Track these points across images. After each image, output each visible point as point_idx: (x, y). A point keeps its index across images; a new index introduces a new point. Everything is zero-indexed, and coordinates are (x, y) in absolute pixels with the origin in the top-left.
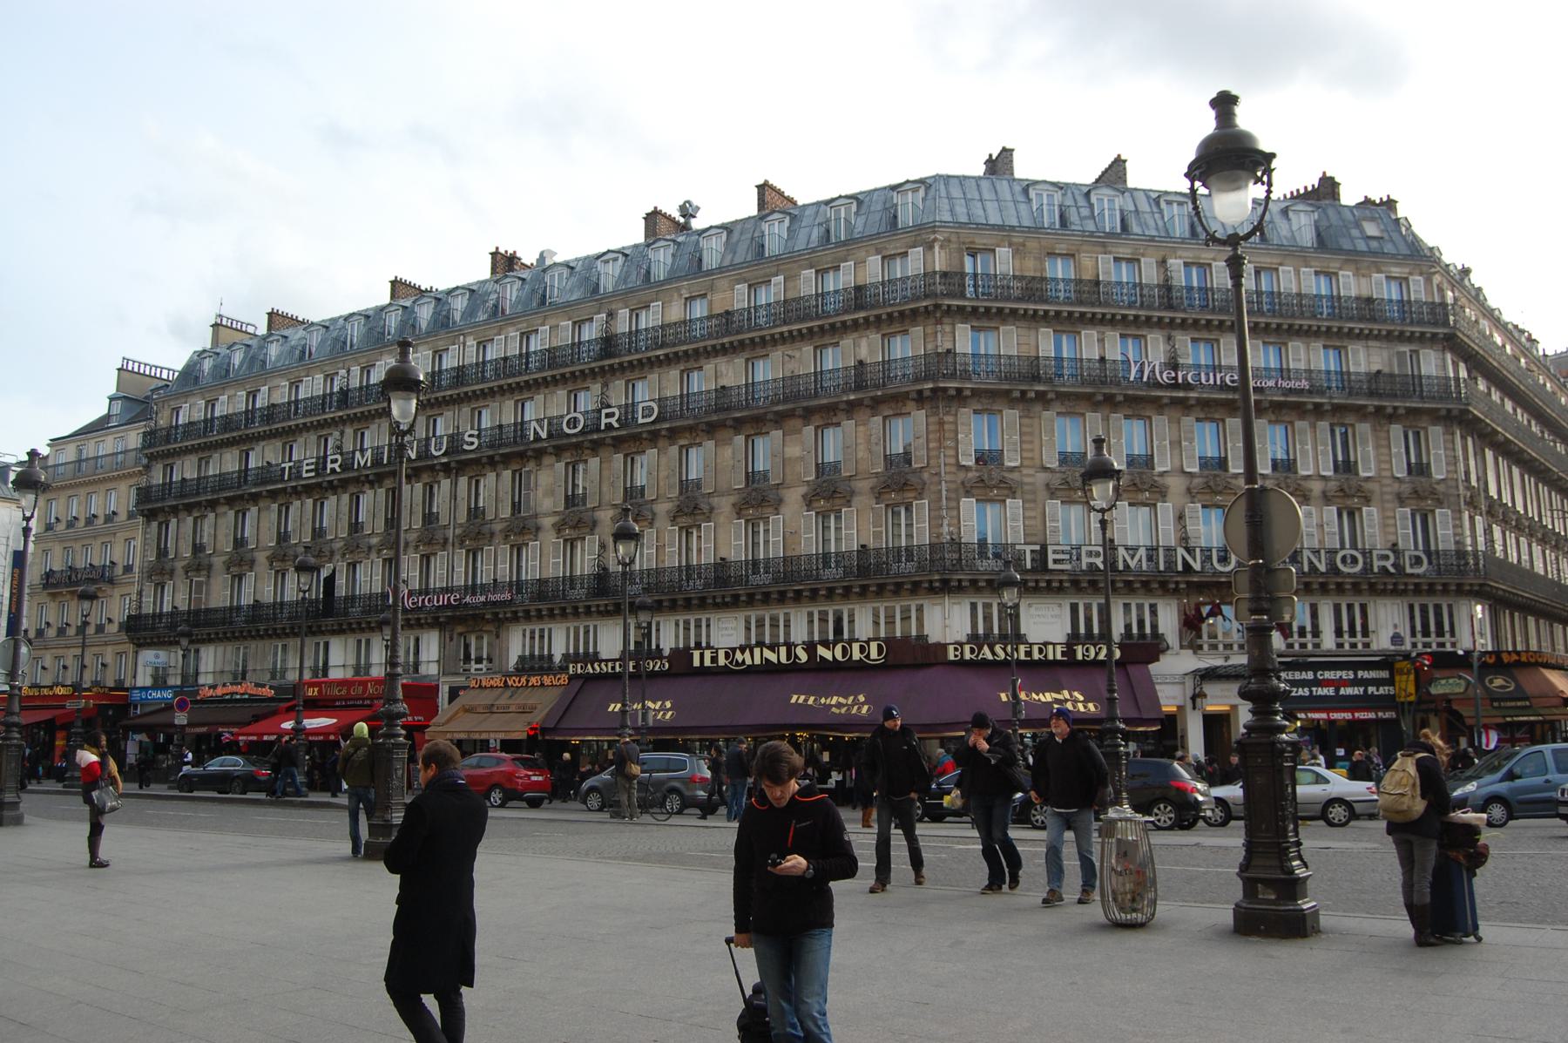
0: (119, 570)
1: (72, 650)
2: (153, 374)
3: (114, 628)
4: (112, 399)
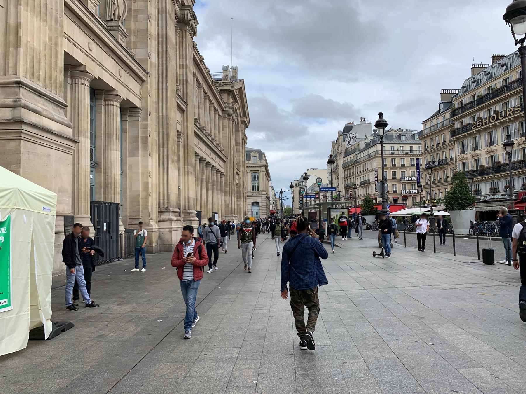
0: (449, 160)
1: (437, 188)
2: (453, 92)
3: (449, 179)
4: (439, 104)
